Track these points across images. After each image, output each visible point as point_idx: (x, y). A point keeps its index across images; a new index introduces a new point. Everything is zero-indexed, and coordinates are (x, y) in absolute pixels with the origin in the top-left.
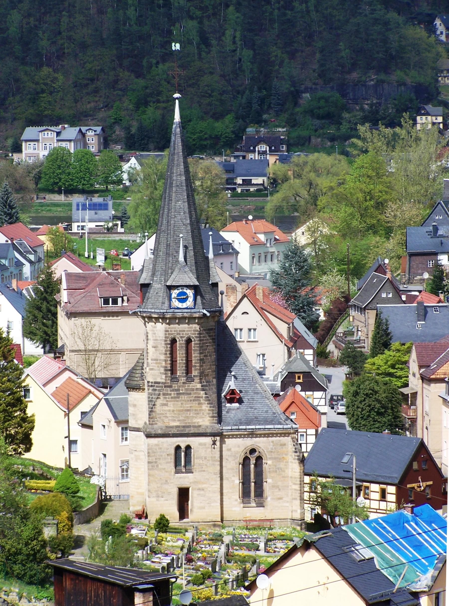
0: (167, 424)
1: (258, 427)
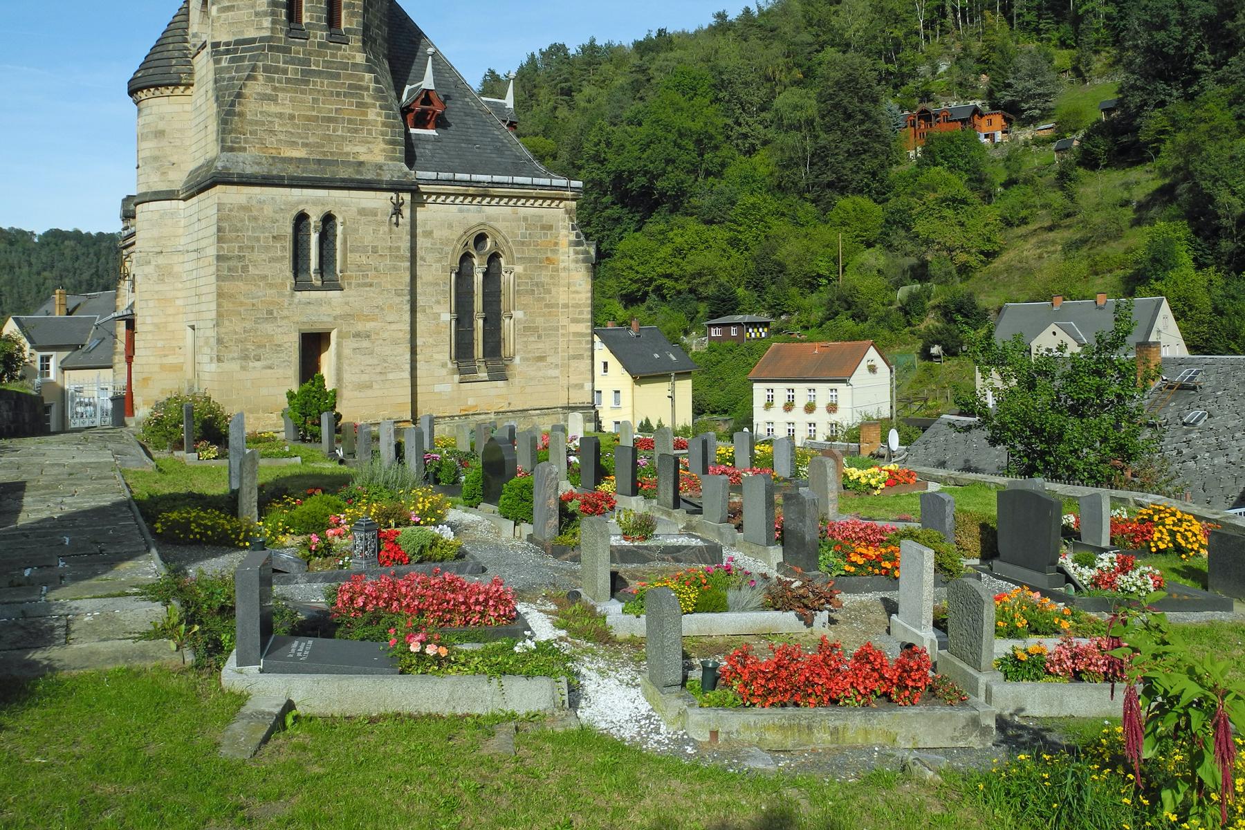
1: (497, 178)
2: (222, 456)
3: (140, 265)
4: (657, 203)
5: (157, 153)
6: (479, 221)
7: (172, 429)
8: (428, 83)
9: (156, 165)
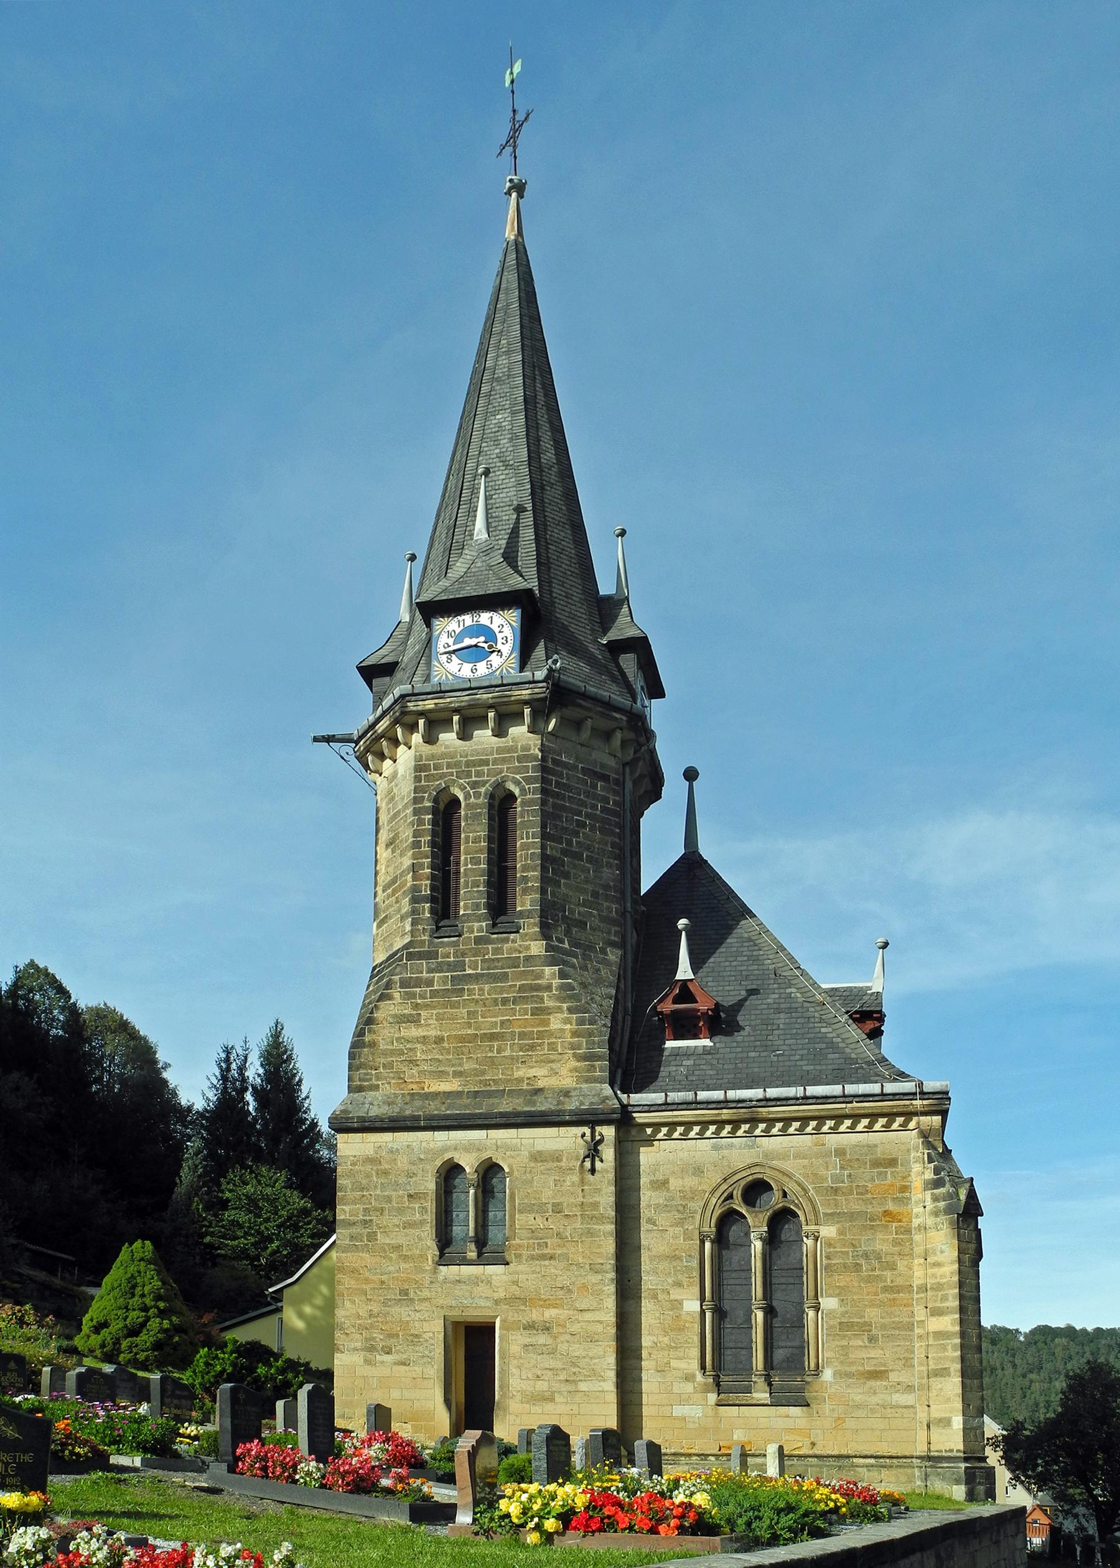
1: (772, 1092)
6: (749, 1161)
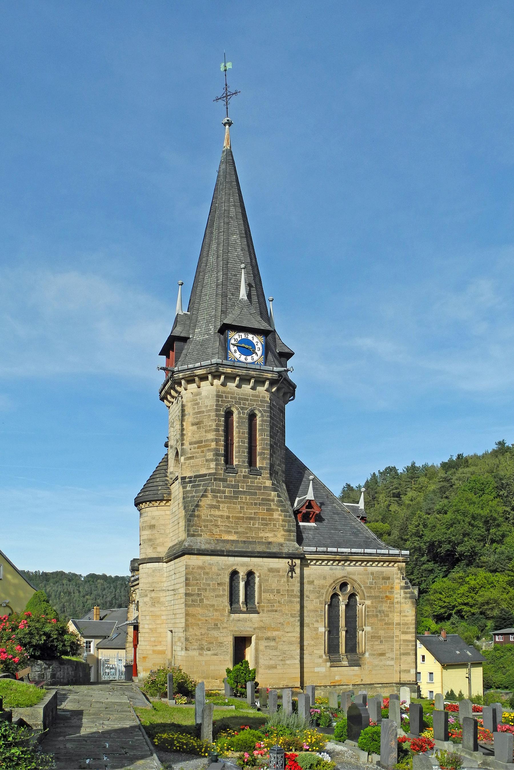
0: (218, 537)
1: (354, 550)
2: (190, 703)
3: (141, 596)
4: (458, 560)
5: (151, 537)
7: (161, 686)
8: (310, 496)
9: (150, 543)
